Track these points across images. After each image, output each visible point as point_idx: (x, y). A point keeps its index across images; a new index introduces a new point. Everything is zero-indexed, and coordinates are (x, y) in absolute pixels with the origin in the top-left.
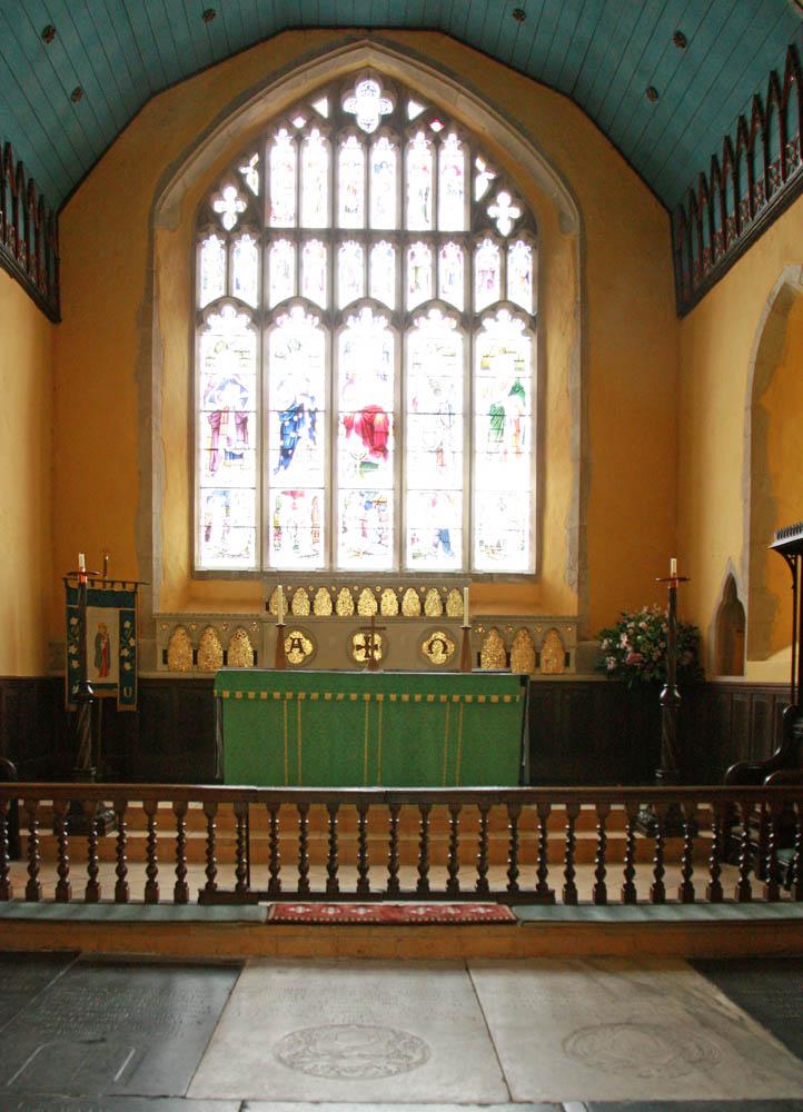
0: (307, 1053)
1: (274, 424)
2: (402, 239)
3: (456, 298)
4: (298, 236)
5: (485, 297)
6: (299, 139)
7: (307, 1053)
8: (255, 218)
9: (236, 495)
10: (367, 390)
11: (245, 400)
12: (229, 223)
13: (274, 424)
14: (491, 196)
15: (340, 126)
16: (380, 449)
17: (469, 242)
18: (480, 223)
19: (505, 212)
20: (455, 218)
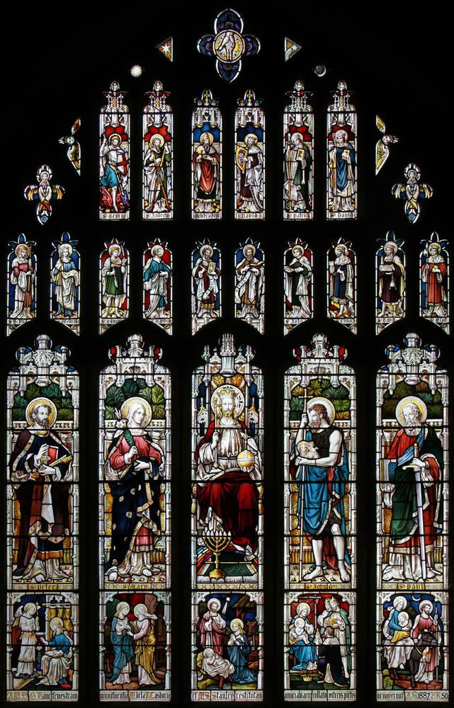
0: (317, 506)
1: (105, 501)
2: (273, 234)
3: (161, 318)
4: (137, 234)
5: (112, 311)
6: (136, 100)
7: (317, 506)
8: (80, 217)
9: (54, 601)
10: (229, 450)
11: (64, 468)
12: (43, 216)
13: (105, 501)
14: (394, 172)
15: (191, 80)
16: (245, 533)
17: (362, 234)
18: (378, 209)
19: (412, 192)
20: (343, 204)
